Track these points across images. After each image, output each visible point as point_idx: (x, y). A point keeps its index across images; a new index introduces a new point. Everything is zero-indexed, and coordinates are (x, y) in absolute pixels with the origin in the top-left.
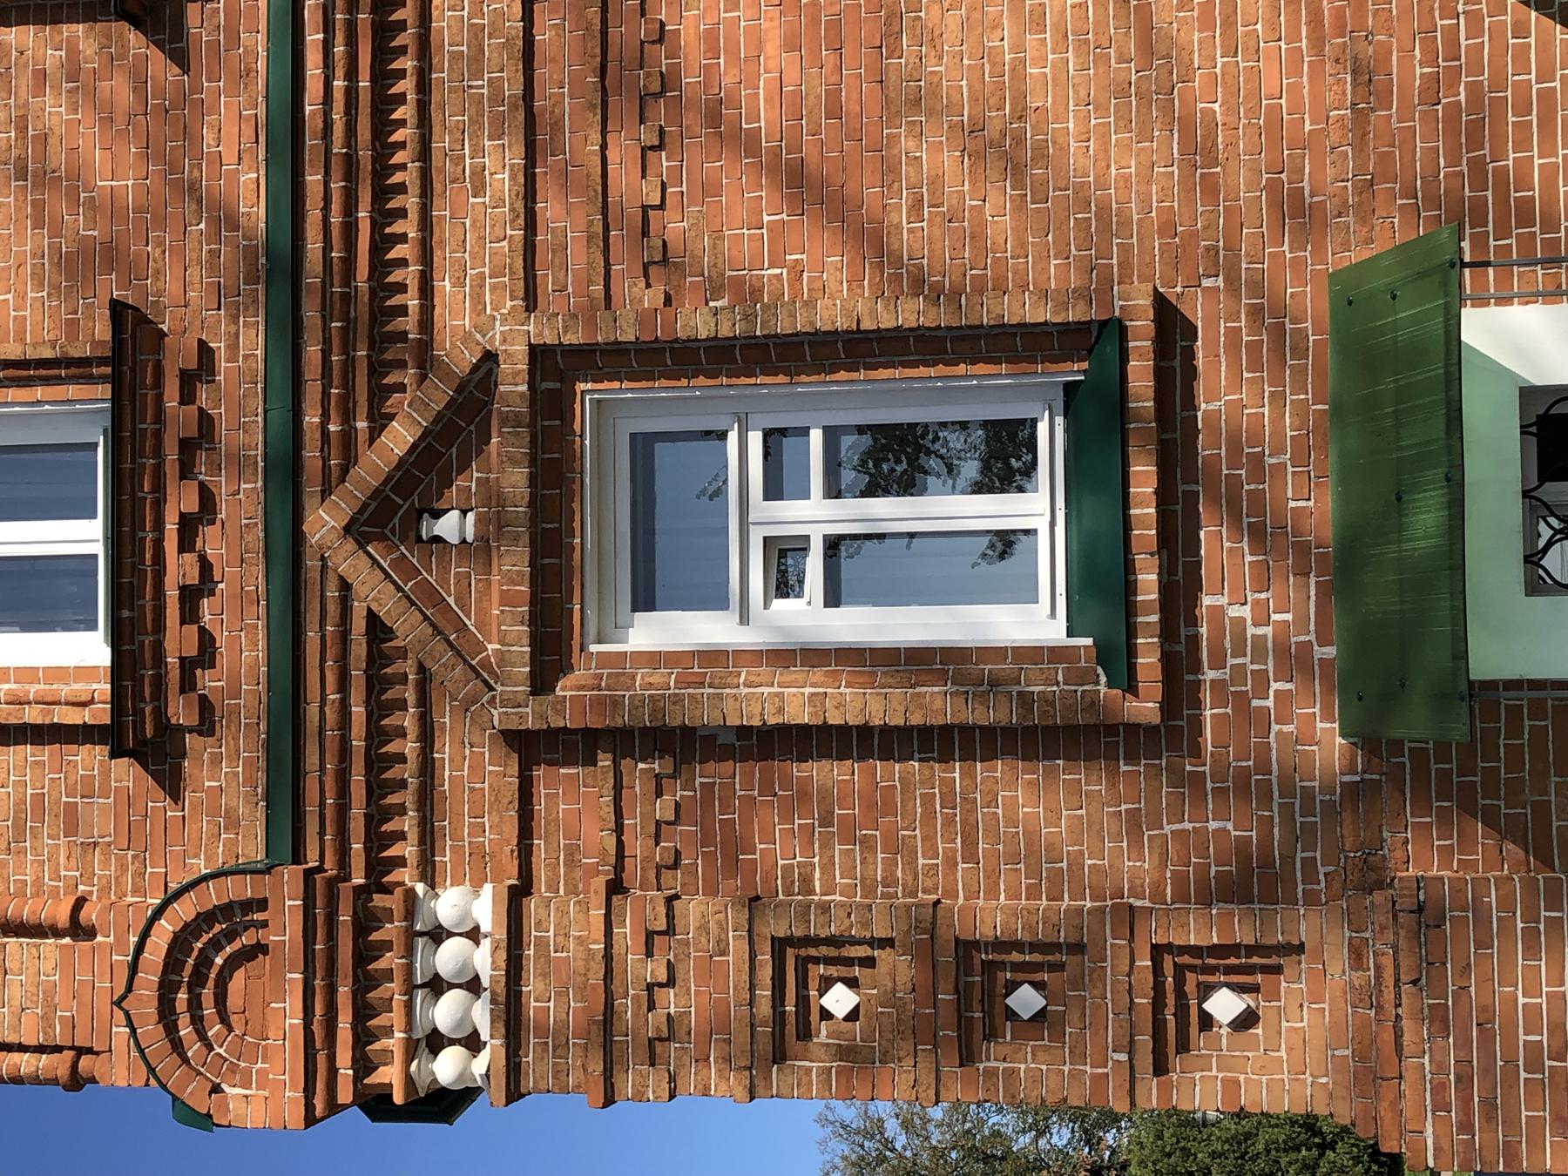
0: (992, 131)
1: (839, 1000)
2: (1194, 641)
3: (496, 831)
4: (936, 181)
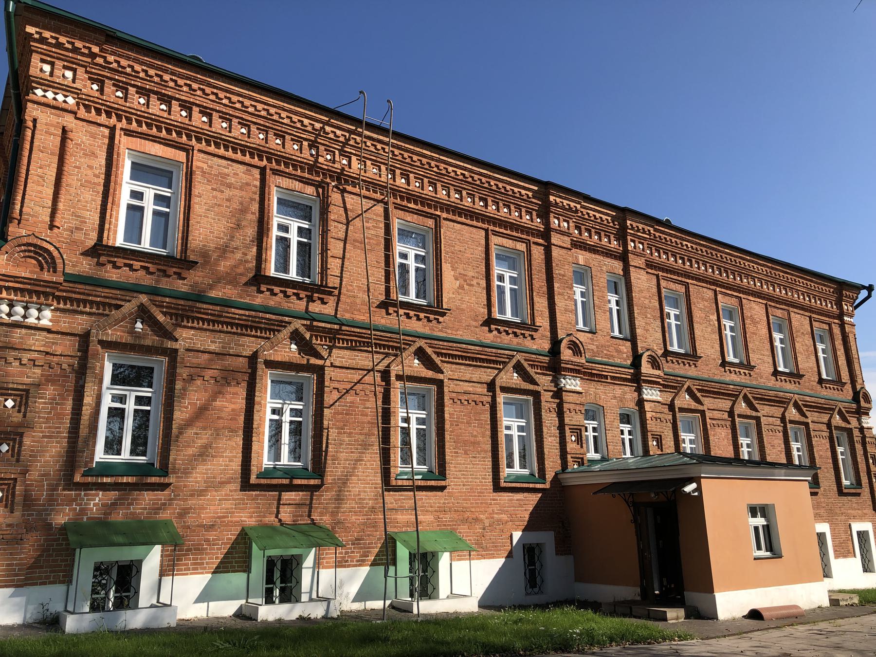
0: (210, 450)
1: (10, 403)
2: (92, 490)
3: (64, 326)
4: (201, 438)
